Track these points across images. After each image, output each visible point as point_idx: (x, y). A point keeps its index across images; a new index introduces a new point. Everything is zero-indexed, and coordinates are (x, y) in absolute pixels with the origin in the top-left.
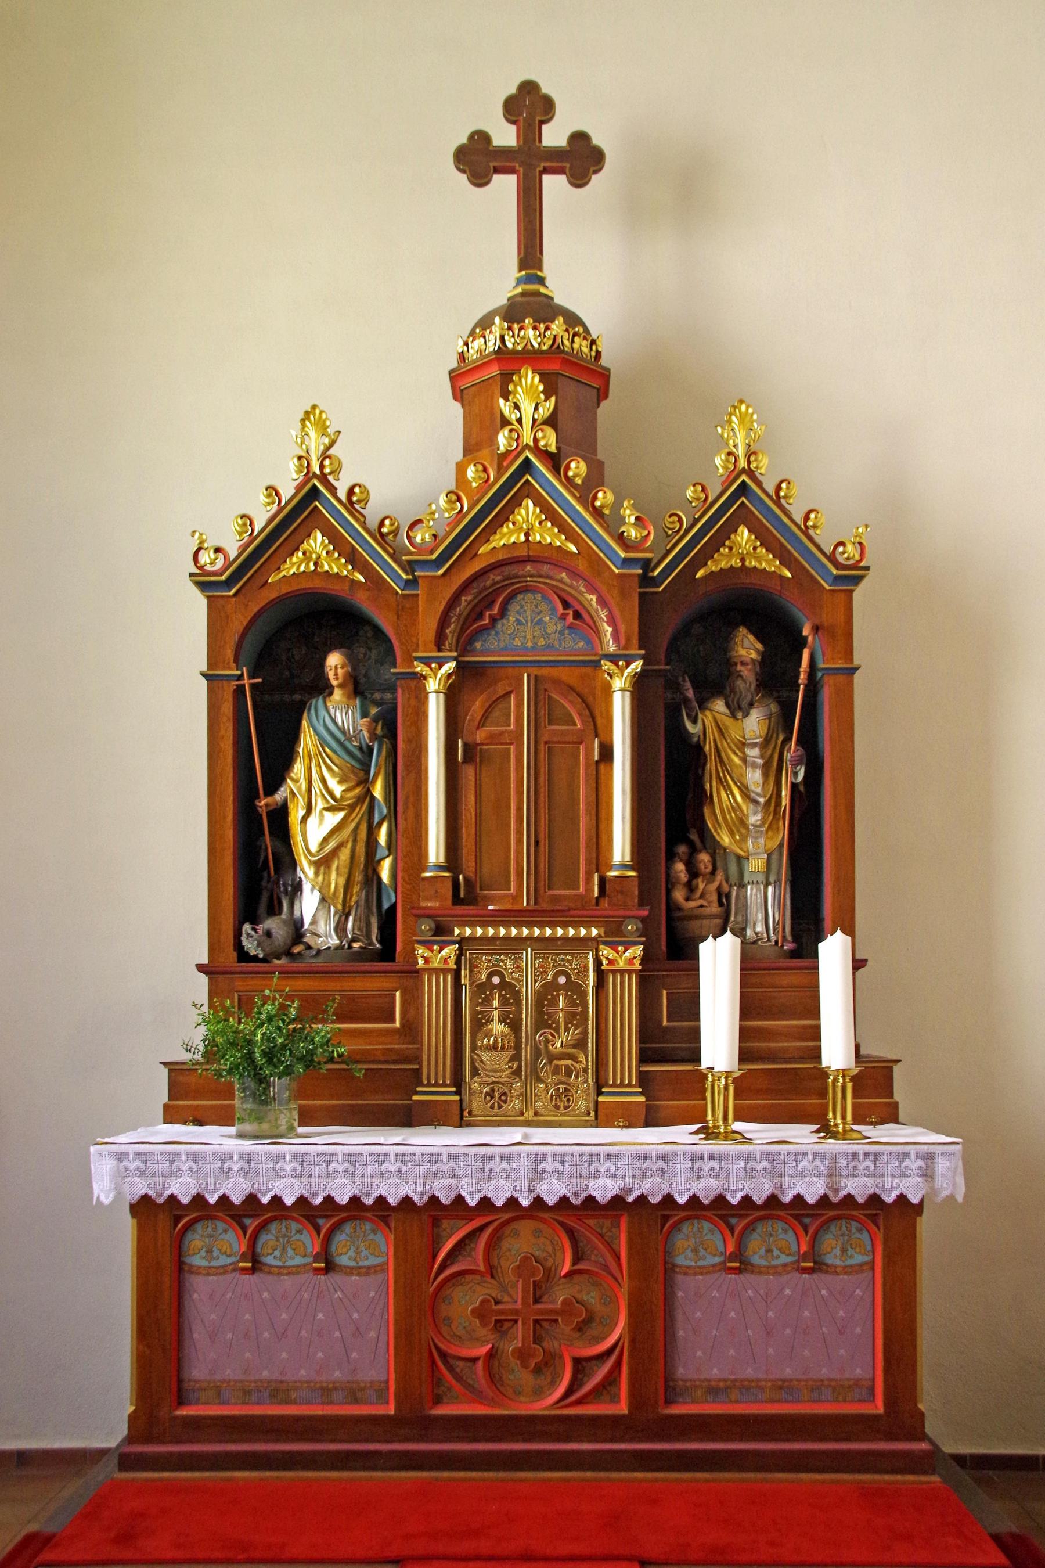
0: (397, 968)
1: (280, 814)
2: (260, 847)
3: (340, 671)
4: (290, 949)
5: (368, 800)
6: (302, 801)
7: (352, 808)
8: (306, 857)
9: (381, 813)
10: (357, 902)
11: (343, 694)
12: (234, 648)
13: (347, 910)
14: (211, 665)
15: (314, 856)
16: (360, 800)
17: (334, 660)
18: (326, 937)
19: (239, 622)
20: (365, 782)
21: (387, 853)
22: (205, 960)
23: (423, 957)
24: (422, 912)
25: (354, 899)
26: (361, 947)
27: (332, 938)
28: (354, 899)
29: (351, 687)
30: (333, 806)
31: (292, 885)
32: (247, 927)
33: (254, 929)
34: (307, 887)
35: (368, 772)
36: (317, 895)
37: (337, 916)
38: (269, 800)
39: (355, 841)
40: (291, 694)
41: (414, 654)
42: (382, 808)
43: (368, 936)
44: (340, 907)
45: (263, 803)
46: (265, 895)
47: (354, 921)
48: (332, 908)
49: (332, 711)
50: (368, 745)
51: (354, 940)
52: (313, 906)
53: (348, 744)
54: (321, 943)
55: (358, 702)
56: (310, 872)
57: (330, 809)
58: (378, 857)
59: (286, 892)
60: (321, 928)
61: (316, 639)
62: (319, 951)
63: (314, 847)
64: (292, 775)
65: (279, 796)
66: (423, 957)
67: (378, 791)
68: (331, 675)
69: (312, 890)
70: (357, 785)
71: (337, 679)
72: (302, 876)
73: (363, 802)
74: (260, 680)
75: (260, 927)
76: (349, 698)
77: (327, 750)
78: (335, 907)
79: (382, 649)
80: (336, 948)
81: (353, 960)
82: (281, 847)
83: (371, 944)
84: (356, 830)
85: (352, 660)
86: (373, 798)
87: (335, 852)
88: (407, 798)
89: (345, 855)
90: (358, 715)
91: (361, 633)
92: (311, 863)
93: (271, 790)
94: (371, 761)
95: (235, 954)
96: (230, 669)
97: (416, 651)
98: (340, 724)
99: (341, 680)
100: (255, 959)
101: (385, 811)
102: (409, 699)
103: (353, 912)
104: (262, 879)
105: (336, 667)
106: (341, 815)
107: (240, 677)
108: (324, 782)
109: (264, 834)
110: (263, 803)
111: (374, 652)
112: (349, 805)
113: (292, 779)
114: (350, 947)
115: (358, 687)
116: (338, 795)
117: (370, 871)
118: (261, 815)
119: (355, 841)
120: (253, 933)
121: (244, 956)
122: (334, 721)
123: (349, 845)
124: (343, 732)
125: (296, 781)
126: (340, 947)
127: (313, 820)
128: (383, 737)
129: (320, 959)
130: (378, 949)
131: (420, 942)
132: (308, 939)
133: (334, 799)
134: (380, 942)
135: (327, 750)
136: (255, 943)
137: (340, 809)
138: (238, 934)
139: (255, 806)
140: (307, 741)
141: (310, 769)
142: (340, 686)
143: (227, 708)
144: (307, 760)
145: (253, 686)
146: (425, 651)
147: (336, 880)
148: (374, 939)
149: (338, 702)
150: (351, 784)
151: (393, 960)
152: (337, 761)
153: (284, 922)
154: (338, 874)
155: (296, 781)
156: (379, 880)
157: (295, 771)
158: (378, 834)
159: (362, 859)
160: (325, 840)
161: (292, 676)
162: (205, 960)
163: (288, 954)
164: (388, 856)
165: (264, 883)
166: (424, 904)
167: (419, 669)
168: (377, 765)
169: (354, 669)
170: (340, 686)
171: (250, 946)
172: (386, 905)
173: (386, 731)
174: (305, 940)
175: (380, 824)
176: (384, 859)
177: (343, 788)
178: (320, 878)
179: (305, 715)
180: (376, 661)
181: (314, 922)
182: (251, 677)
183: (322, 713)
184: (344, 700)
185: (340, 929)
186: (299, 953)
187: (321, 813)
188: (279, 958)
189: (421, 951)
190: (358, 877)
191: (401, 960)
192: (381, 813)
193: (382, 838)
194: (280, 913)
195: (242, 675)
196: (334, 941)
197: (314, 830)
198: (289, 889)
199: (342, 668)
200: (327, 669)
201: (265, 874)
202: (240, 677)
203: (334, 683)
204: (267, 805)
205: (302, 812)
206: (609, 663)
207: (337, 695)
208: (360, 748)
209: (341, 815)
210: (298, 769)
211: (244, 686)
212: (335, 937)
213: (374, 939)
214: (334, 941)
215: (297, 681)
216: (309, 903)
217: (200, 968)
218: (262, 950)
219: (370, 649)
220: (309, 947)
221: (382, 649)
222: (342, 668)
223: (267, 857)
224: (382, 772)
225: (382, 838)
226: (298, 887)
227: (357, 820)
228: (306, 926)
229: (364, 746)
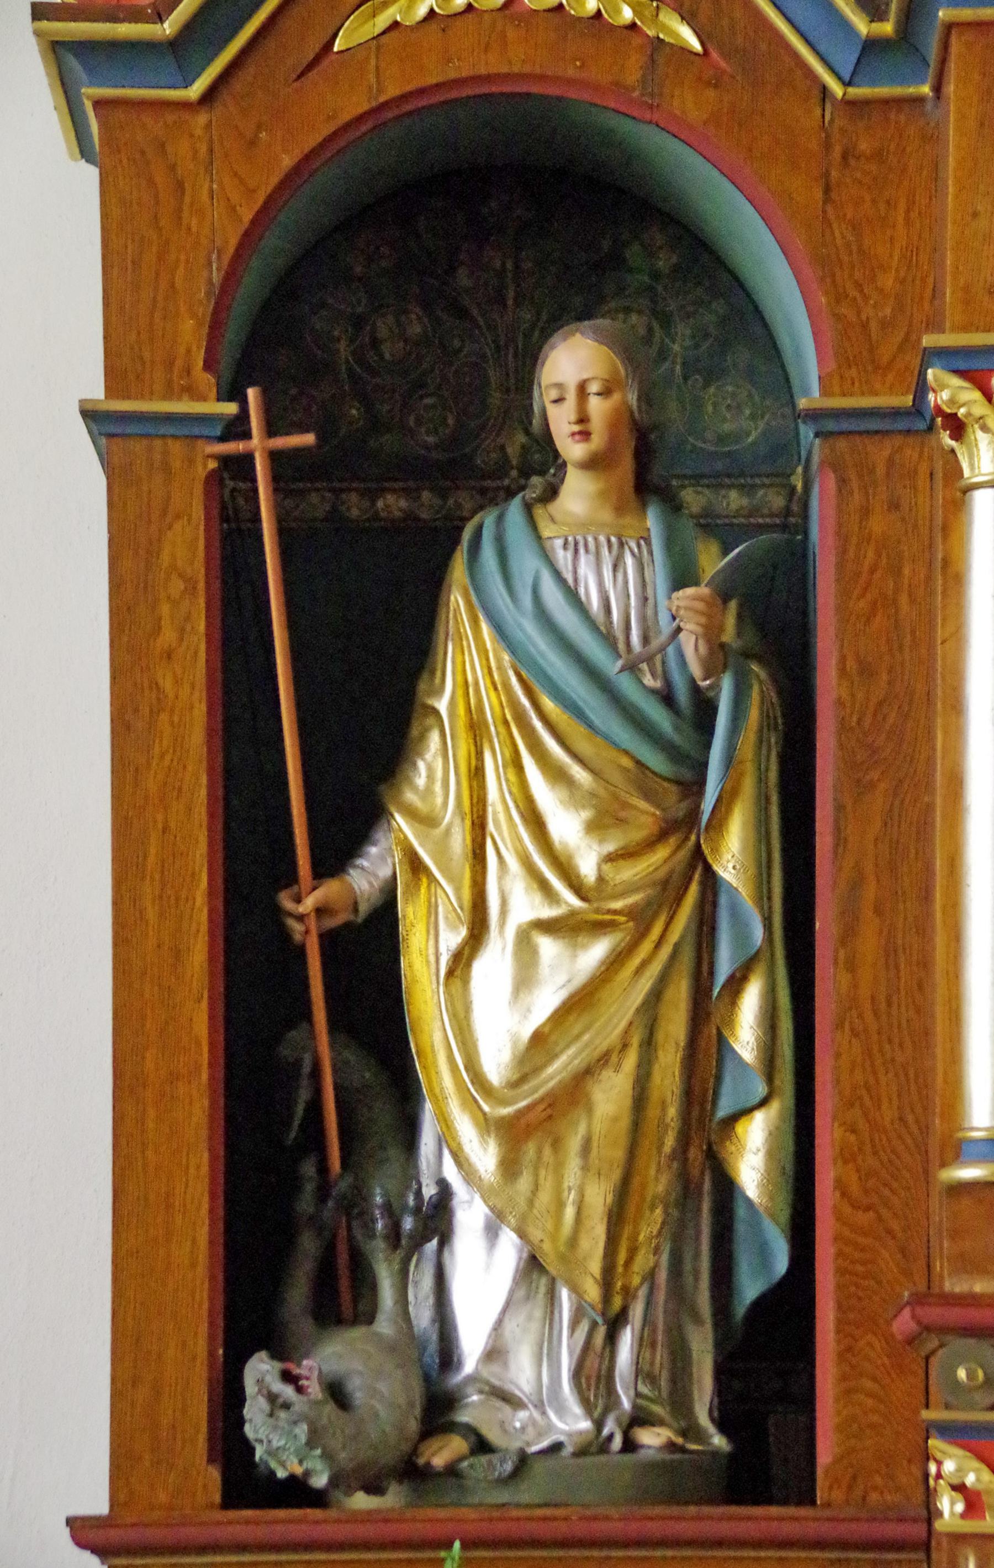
0: (826, 1530)
1: (370, 944)
2: (298, 1064)
3: (596, 405)
4: (415, 1452)
5: (694, 889)
6: (450, 895)
7: (641, 919)
8: (470, 1104)
9: (741, 934)
10: (651, 1277)
11: (603, 495)
12: (206, 310)
13: (617, 1302)
14: (116, 378)
15: (504, 1102)
16: (667, 892)
17: (573, 365)
18: (540, 1406)
19: (222, 209)
20: (686, 826)
21: (761, 1089)
22: (97, 1502)
23: (960, 1488)
24: (955, 1315)
25: (643, 1261)
26: (671, 1446)
27: (561, 1410)
28: (643, 1261)
29: (627, 464)
30: (573, 913)
31: (417, 1210)
32: (260, 1370)
33: (288, 1377)
34: (470, 1215)
35: (695, 787)
36: (509, 1249)
37: (584, 1327)
38: (329, 890)
39: (649, 1044)
40: (372, 495)
41: (928, 340)
42: (748, 918)
43: (680, 1403)
44: (593, 1292)
45: (309, 903)
46: (308, 1245)
47: (642, 1343)
48: (565, 1294)
49: (563, 558)
50: (695, 689)
51: (639, 1419)
52: (499, 1294)
53: (626, 685)
54: (517, 1430)
55: (653, 520)
56: (485, 1157)
57: (564, 928)
58: (724, 1108)
59: (394, 1236)
60: (522, 1373)
61: (463, 278)
62: (523, 1460)
63: (496, 1062)
64: (410, 796)
65: (368, 873)
66: (960, 1488)
67: (733, 856)
68: (561, 422)
69: (492, 1232)
70: (662, 836)
71: (585, 435)
72: (450, 1172)
73: (679, 900)
74: (309, 439)
75: (308, 1367)
76: (620, 510)
77: (548, 704)
78: (575, 1290)
79: (709, 319)
80: (582, 1452)
81: (673, 1498)
82: (366, 1073)
83: (690, 1431)
84: (656, 996)
85: (638, 357)
86: (711, 881)
87: (574, 1092)
88: (857, 884)
89: (610, 1096)
90: (659, 576)
91: (633, 254)
92: (486, 1125)
93: (335, 856)
94: (708, 746)
95: (214, 1474)
96: (192, 392)
97: (935, 325)
98: (595, 603)
99: (598, 441)
100: (296, 1492)
101: (758, 933)
102: (866, 512)
103: (637, 1311)
104: (295, 1185)
105: (582, 389)
106: (596, 952)
107: (237, 428)
108: (536, 821)
109: (307, 1015)
110: (309, 903)
111: (683, 330)
112: (632, 913)
113: (412, 814)
114: (630, 1446)
115: (648, 468)
116: (588, 867)
117: (695, 1154)
118: (301, 952)
119: (649, 1044)
120: (288, 1391)
121: (247, 1483)
122: (572, 595)
123: (631, 1060)
124: (608, 639)
125: (425, 821)
126: (595, 1446)
127: (493, 967)
128: (747, 655)
129: (526, 1493)
130: (715, 1454)
131: (952, 1432)
132: (474, 1410)
133: (577, 887)
134: (723, 1425)
135: (548, 704)
136: (302, 1431)
137: (599, 928)
138: (228, 1398)
139: (277, 913)
140: (468, 667)
141: (477, 773)
142: (592, 464)
143: (187, 545)
144: (464, 746)
145: (275, 457)
146: (965, 328)
147: (581, 1192)
148: (704, 1420)
149: (584, 525)
150: (637, 835)
151: (804, 1494)
152: (584, 746)
153: (392, 1348)
154: (585, 1168)
155: (425, 821)
156: (726, 1187)
157: (421, 781)
158: (730, 1019)
159: (672, 1112)
160: (540, 1044)
161: (375, 425)
162: (97, 1502)
163: (412, 1472)
164: (763, 1103)
165: (305, 1203)
166: (955, 1285)
167: (945, 395)
168: (730, 760)
169: (646, 398)
170: (592, 464)
171: (277, 1442)
172: (750, 1288)
173: (751, 637)
174: (464, 1417)
175: (736, 984)
176: (747, 1111)
177: (610, 847)
178: (524, 1183)
179: (458, 570)
180: (689, 368)
181: (495, 1353)
182: (271, 430)
183: (526, 563)
184: (606, 515)
185: (593, 1380)
186: (452, 1471)
187: (524, 941)
188: (374, 1489)
189: (952, 1463)
190: (658, 1182)
191: (838, 1495)
192: (741, 934)
193: (745, 1036)
194: (370, 1318)
195: (243, 415)
196: (572, 1423)
197: (495, 998)
198: (408, 1223)
199: (605, 393)
200: (544, 395)
201: (309, 1168)
202: (237, 428)
203: (573, 450)
204: (321, 911)
205: (452, 938)
206: (956, 381)
207: (578, 495)
208: (667, 698)
209: (596, 952)
210: (433, 773)
211: (248, 459)
212: (577, 1409)
213: (704, 1420)
214: (572, 1423)
215: (388, 441)
216: (480, 1276)
217: (83, 1531)
218: (328, 1456)
219: (666, 321)
220: (482, 1446)
221: (709, 319)
222: (605, 393)
223: (315, 1107)
224: (748, 786)
225: (745, 1036)
226: (437, 1219)
227: (655, 968)
228: (469, 1365)
229: (683, 696)
